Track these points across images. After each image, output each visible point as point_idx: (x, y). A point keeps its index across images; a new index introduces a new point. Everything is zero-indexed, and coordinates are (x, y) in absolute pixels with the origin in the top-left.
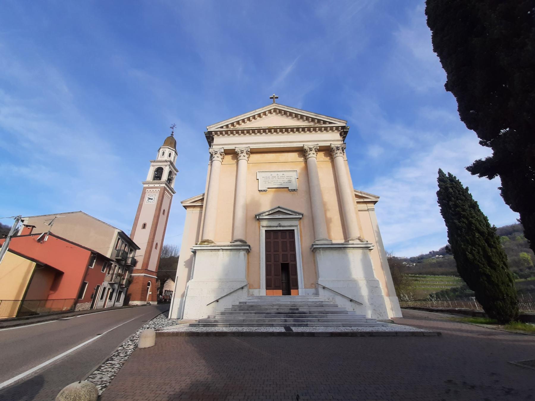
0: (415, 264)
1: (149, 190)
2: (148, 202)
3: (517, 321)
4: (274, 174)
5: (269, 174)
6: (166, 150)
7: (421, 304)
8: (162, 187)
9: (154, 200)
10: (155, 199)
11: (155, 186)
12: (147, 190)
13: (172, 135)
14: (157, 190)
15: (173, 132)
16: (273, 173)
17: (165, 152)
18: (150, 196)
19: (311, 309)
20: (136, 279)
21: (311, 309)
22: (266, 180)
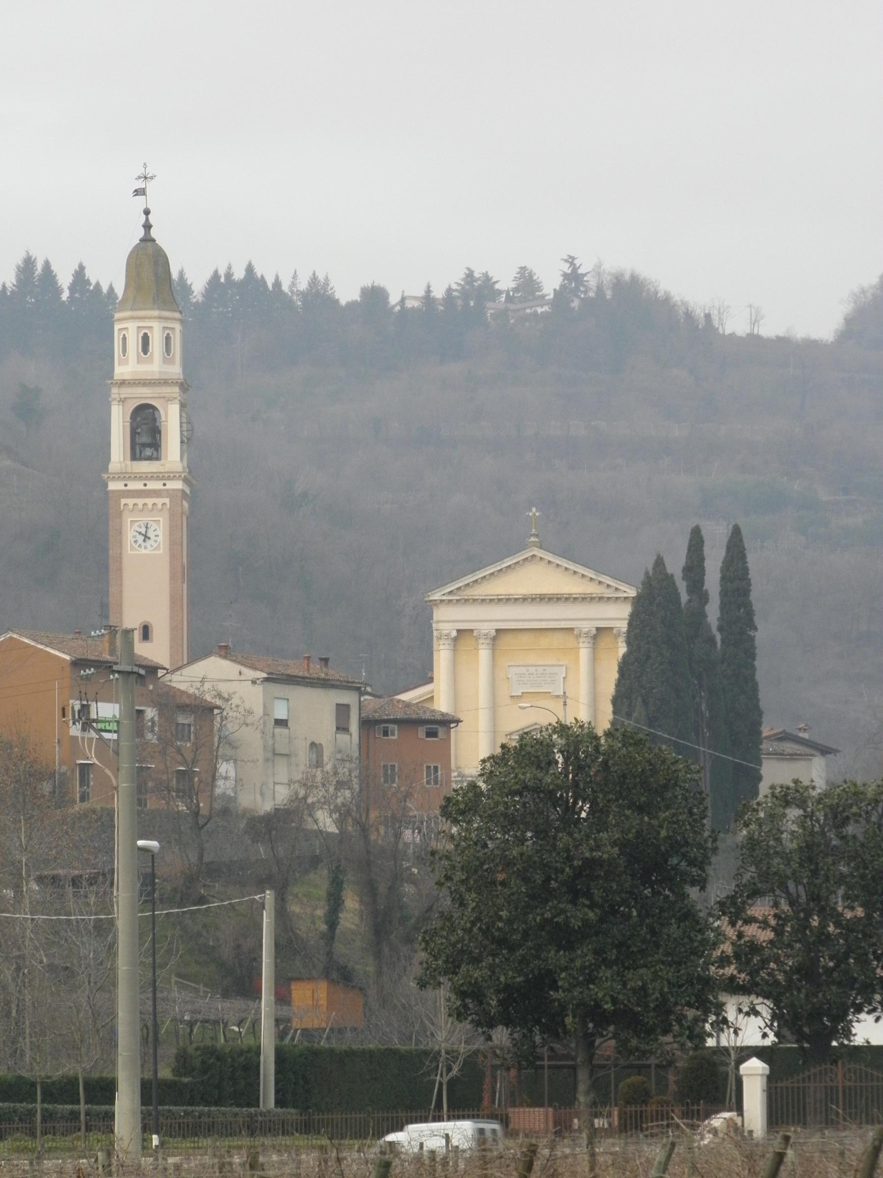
0: (622, 909)
1: (130, 502)
2: (136, 546)
3: (642, 282)
4: (532, 670)
5: (523, 670)
6: (151, 327)
7: (585, 811)
8: (173, 490)
9: (156, 541)
10: (157, 536)
11: (129, 487)
12: (123, 501)
13: (147, 227)
14: (159, 501)
15: (147, 212)
16: (530, 668)
17: (171, 335)
18: (138, 524)
19: (150, 391)
20: (274, 766)
21: (150, 391)
22: (519, 679)
